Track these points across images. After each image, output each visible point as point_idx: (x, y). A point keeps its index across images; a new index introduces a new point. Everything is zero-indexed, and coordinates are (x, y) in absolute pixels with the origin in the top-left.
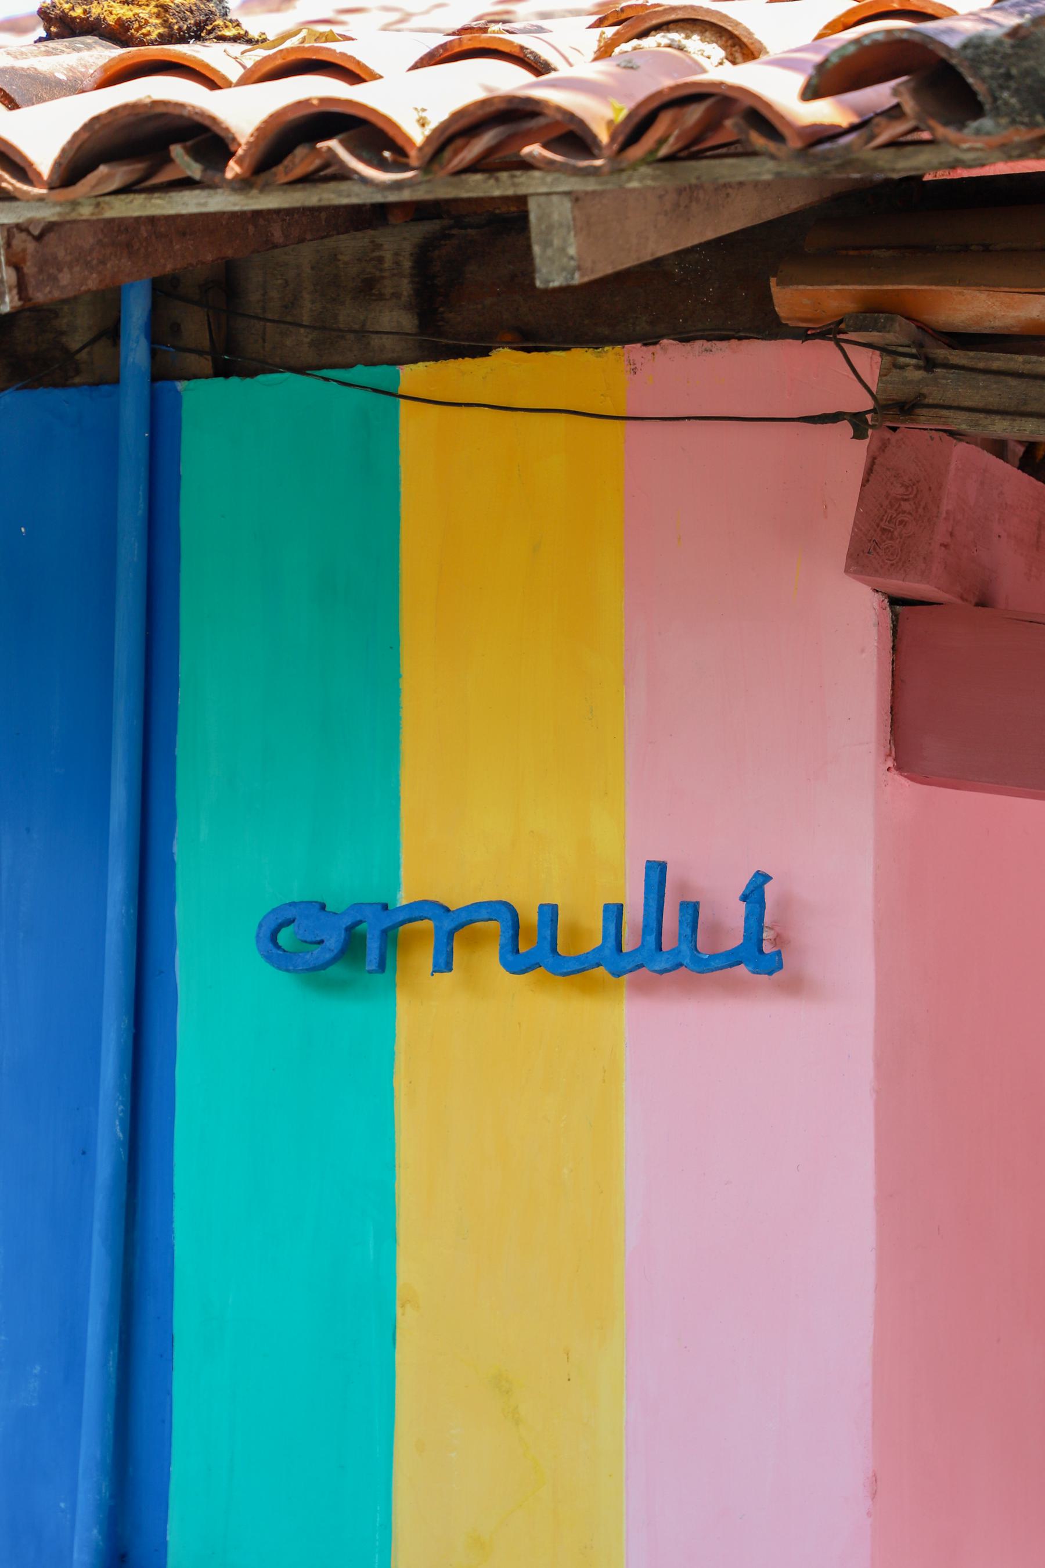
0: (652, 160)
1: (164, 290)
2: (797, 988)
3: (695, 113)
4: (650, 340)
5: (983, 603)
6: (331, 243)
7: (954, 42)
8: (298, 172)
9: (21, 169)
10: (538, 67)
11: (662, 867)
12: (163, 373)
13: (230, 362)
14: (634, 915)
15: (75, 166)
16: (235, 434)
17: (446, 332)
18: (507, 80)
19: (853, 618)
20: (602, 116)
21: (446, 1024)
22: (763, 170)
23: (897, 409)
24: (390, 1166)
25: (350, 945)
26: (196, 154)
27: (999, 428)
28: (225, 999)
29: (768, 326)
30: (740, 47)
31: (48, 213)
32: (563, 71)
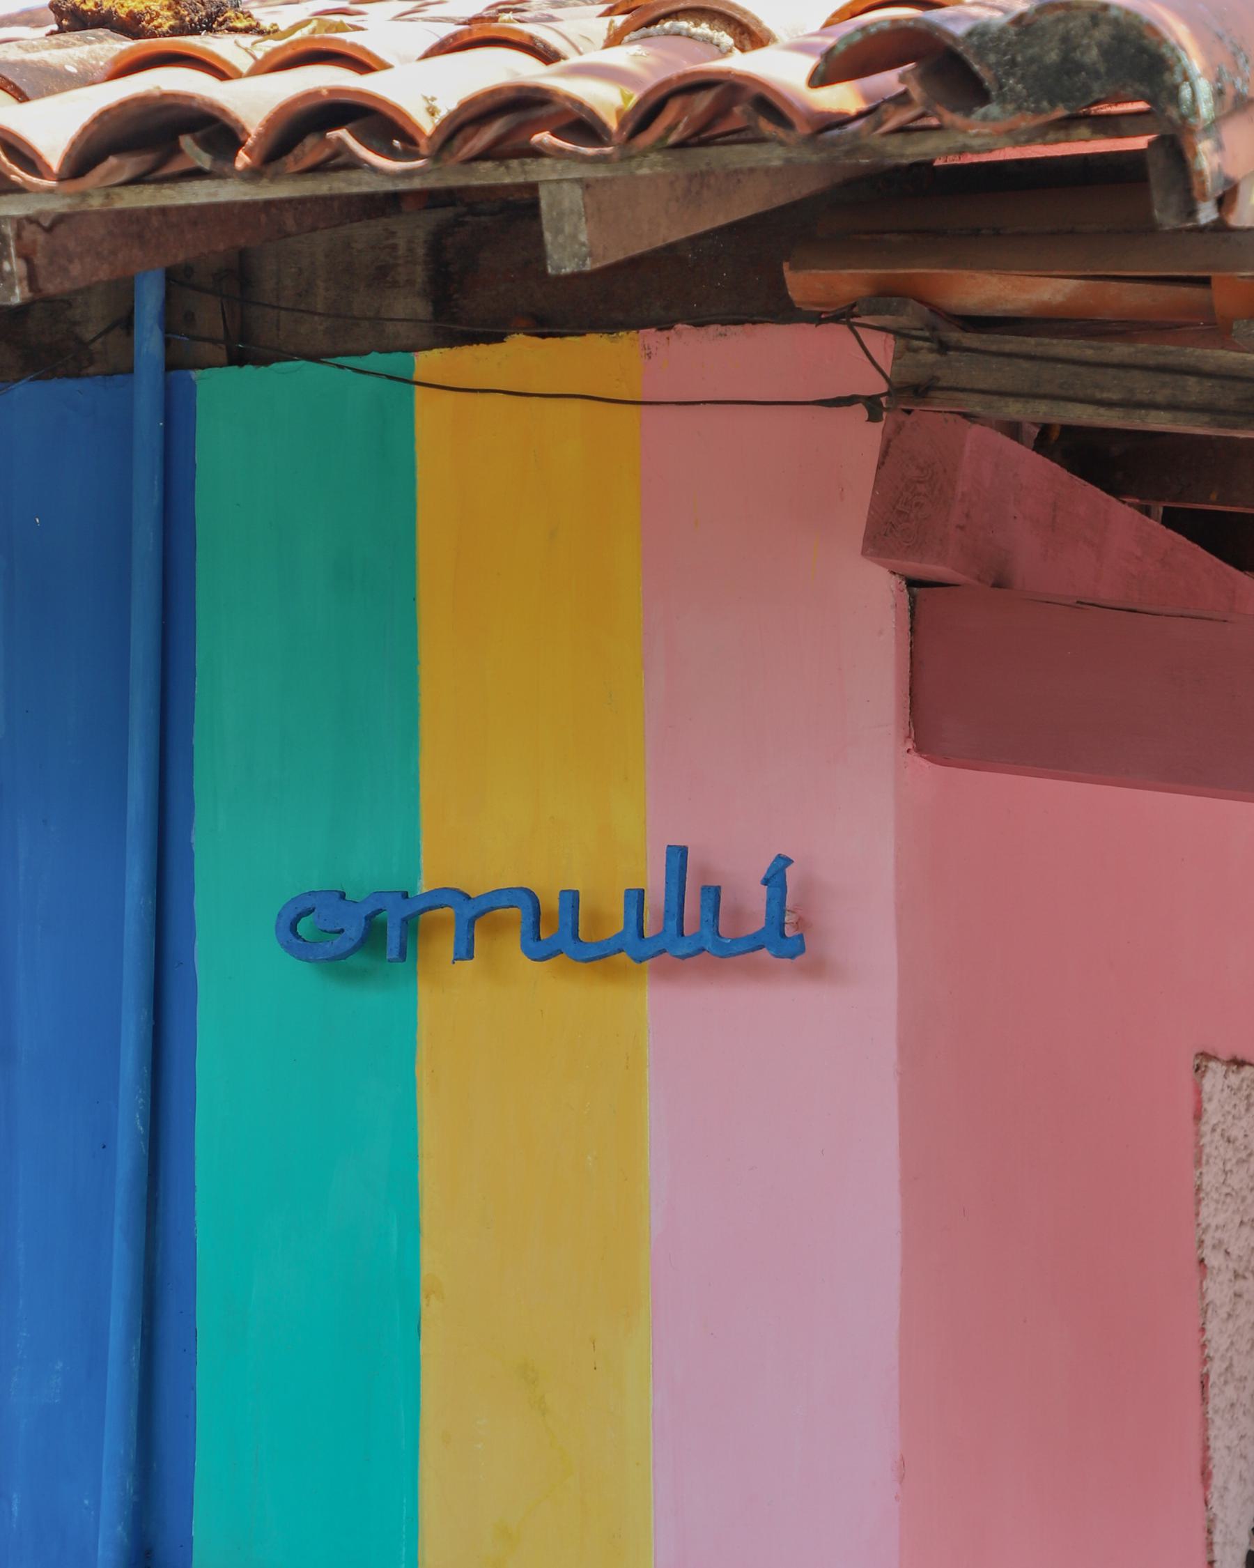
0: (661, 146)
1: (175, 279)
2: (818, 970)
3: (703, 101)
4: (664, 325)
5: (1000, 583)
7: (959, 30)
8: (309, 161)
10: (547, 56)
11: (683, 851)
13: (244, 351)
14: (655, 900)
15: (87, 156)
18: (527, 70)
19: (875, 594)
21: (464, 1007)
22: (773, 156)
23: (910, 392)
25: (369, 934)
26: (206, 144)
27: (1014, 410)
29: (783, 311)
31: (58, 205)
32: (574, 59)
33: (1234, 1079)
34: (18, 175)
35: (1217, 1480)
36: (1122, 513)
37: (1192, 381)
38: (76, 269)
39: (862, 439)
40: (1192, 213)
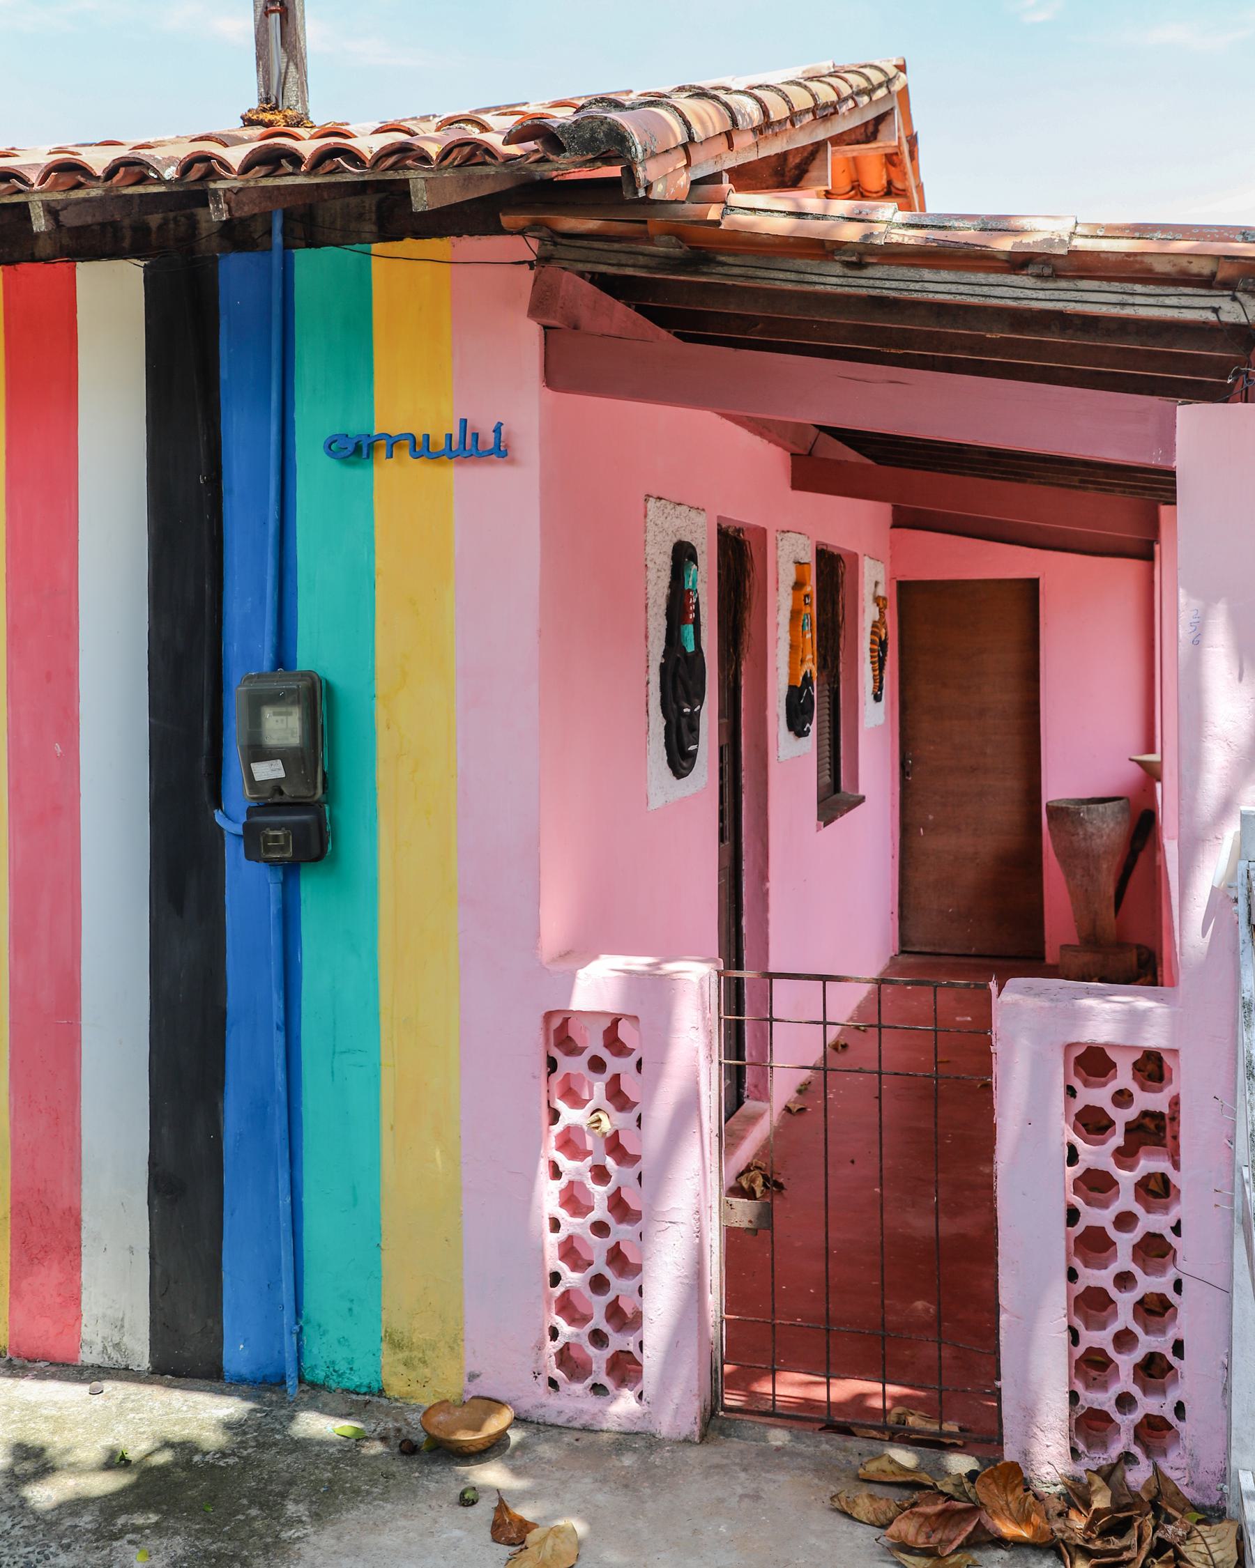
0: (451, 166)
1: (287, 216)
2: (512, 462)
3: (467, 150)
4: (459, 235)
5: (576, 328)
6: (347, 200)
7: (555, 126)
8: (327, 169)
9: (227, 167)
10: (412, 134)
11: (466, 421)
12: (288, 246)
13: (312, 242)
14: (456, 438)
15: (247, 167)
16: (314, 268)
17: (388, 234)
18: (402, 137)
19: (532, 331)
20: (433, 150)
21: (391, 476)
22: (491, 170)
23: (544, 260)
24: (372, 527)
25: (357, 450)
26: (291, 163)
27: (581, 267)
28: (314, 470)
29: (501, 231)
30: (484, 128)
31: (239, 184)
32: (422, 135)
33: (658, 504)
34: (223, 173)
35: (650, 639)
36: (619, 306)
37: (640, 258)
38: (246, 209)
39: (527, 277)
40: (636, 193)
